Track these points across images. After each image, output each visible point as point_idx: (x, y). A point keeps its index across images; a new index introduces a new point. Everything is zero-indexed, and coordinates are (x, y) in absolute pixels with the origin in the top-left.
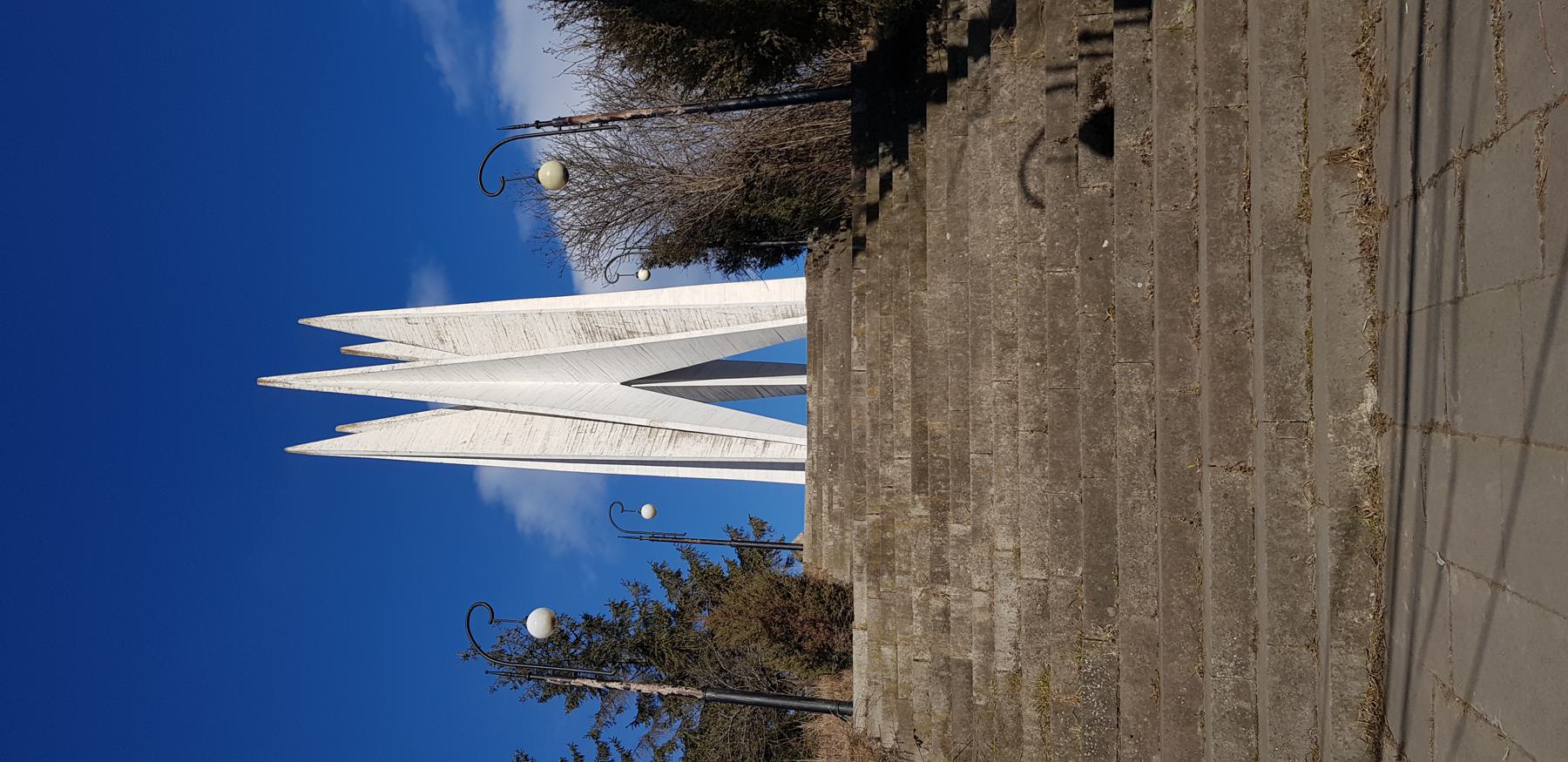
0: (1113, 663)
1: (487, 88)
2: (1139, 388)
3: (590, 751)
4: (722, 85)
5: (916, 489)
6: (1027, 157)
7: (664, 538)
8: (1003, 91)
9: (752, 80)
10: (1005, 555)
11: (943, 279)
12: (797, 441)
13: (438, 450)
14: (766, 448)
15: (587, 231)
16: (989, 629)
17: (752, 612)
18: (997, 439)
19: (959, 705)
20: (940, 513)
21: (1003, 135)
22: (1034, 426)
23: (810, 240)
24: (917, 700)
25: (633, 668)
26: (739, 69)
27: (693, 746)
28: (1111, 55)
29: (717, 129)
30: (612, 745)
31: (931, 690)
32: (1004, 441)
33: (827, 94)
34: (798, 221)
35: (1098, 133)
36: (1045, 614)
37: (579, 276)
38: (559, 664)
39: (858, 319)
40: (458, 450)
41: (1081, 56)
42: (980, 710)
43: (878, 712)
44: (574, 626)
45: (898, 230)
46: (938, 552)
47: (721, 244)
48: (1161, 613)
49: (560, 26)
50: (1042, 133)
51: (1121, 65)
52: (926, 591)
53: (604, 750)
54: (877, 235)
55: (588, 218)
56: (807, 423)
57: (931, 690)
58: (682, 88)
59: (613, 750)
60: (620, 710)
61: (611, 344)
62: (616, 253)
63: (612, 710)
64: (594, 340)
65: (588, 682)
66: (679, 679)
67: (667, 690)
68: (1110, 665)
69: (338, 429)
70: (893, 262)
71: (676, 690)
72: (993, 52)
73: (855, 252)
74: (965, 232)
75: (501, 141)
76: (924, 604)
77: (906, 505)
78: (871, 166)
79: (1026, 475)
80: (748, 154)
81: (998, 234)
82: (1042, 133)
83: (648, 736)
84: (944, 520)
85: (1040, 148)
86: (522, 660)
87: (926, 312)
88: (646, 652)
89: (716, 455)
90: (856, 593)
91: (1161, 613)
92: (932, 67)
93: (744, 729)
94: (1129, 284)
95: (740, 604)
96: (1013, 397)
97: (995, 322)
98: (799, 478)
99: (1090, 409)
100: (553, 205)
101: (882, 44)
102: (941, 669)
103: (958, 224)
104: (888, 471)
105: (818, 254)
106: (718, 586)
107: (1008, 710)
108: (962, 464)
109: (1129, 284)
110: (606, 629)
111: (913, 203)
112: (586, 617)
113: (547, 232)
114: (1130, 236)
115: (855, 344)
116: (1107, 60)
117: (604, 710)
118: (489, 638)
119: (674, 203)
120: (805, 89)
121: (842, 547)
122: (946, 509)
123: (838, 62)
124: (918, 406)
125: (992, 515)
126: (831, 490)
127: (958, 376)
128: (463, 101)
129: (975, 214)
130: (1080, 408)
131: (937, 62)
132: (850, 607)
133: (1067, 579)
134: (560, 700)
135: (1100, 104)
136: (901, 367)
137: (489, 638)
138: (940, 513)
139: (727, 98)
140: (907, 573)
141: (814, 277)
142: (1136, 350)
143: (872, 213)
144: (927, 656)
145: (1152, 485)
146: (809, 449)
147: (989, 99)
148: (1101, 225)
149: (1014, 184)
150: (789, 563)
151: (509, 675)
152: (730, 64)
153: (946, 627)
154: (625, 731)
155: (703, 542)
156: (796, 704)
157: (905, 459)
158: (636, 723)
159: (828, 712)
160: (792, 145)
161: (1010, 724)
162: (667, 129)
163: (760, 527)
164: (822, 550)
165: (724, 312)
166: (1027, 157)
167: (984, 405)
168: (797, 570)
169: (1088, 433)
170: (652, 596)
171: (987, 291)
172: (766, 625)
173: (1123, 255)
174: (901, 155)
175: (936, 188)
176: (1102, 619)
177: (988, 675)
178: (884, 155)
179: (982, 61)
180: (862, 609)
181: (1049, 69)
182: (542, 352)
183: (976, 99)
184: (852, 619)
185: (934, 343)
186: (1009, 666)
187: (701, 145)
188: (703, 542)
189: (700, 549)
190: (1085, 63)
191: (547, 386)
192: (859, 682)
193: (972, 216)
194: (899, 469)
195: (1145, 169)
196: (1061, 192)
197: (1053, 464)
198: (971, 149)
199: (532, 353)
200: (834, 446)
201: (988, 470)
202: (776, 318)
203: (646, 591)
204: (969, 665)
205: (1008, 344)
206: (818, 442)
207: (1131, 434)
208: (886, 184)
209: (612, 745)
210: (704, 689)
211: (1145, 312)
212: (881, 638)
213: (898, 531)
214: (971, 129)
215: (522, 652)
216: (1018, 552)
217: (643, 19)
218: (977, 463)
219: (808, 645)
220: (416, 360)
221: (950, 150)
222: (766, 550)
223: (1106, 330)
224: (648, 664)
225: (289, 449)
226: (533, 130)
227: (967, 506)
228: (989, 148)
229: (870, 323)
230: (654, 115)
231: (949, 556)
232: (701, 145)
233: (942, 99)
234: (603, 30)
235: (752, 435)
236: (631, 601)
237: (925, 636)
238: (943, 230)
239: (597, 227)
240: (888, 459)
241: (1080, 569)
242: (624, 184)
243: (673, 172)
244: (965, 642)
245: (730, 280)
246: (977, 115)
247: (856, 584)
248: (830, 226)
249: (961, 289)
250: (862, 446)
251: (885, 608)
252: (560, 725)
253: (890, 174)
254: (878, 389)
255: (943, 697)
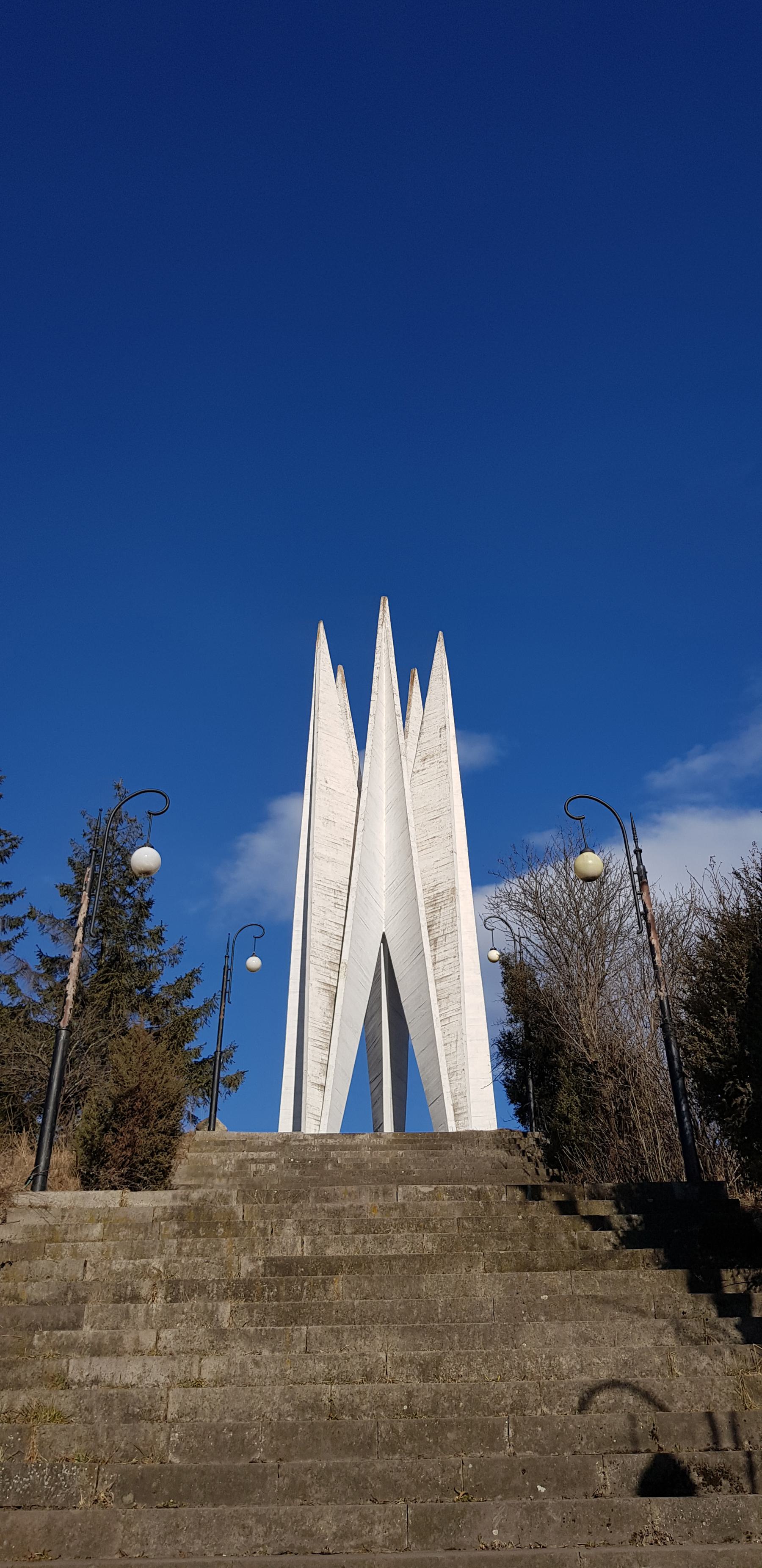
0: (71, 1501)
1: (668, 801)
2: (379, 1533)
3: (16, 910)
4: (691, 1042)
5: (269, 1261)
6: (635, 1389)
7: (226, 981)
8: (705, 1360)
9: (699, 1074)
10: (195, 1368)
11: (498, 1292)
12: (325, 1121)
13: (319, 758)
14: (316, 1095)
15: (536, 898)
16: (115, 1349)
17: (145, 1076)
18: (322, 1359)
19: (35, 1314)
20: (243, 1290)
21: (657, 1360)
22: (337, 1402)
23: (537, 1134)
24: (43, 1264)
25: (96, 951)
26: (709, 1060)
27: (13, 1015)
28: (753, 1492)
29: (647, 1032)
30: (21, 931)
31: (53, 1281)
32: (321, 1366)
33: (689, 1152)
34: (555, 1121)
35: (665, 1478)
36: (129, 1417)
37: (491, 891)
38: (105, 876)
39: (452, 1193)
40: (319, 776)
41: (749, 1455)
42: (27, 1339)
43: (33, 1219)
44: (142, 890)
45: (550, 1237)
46: (198, 1288)
47: (528, 1036)
48: (125, 1561)
49: (737, 874)
50: (662, 1408)
51: (742, 1504)
52: (159, 1275)
53: (16, 923)
54: (543, 1213)
55: (549, 900)
56: (343, 1134)
57: (53, 1281)
58: (685, 997)
59: (15, 932)
60: (55, 938)
61: (424, 923)
62: (515, 927)
63: (55, 931)
64: (427, 905)
65: (84, 908)
66: (81, 999)
67: (71, 989)
68: (69, 1498)
69: (340, 668)
70: (515, 1232)
71: (70, 998)
72: (748, 1347)
73: (524, 1188)
74: (550, 1318)
75: (618, 814)
76: (145, 1273)
77: (252, 1251)
78: (617, 1206)
79: (283, 1394)
80: (623, 1066)
81: (549, 1357)
82: (662, 1408)
83: (26, 968)
84: (235, 1295)
85: (645, 1406)
86: (111, 840)
87: (461, 1271)
88: (111, 964)
89: (310, 1033)
90: (161, 1194)
91: (125, 1561)
92: (727, 1275)
93: (26, 1069)
94: (497, 1519)
95: (155, 1063)
96: (368, 1377)
97: (451, 1356)
98: (285, 1125)
99: (354, 1472)
100: (560, 865)
101: (746, 1216)
102: (75, 1292)
103: (560, 1309)
104: (289, 1230)
105: (523, 1144)
106: (175, 1037)
107: (25, 1372)
108: (293, 1317)
109: (497, 1519)
110: (137, 923)
111: (578, 1255)
112: (150, 903)
113: (534, 860)
114: (550, 1520)
115: (426, 1189)
116: (747, 1487)
117: (56, 922)
118: (135, 809)
119: (568, 987)
120: (694, 1128)
121: (211, 1175)
122: (247, 1297)
123: (725, 1167)
124: (359, 1264)
125: (239, 1352)
126: (271, 1161)
127: (392, 1310)
128: (658, 780)
129: (569, 1329)
130: (357, 1459)
131: (733, 1281)
132: (146, 1186)
133: (167, 1444)
134: (70, 879)
135: (697, 1479)
136: (402, 1243)
137: (135, 809)
138: (243, 1290)
139: (679, 1046)
140: (179, 1253)
141: (499, 1139)
142: (422, 1529)
143: (567, 1207)
144: (89, 1277)
145: (270, 1550)
146: (315, 1136)
147: (696, 1343)
148: (564, 1482)
149: (604, 1375)
150: (194, 1119)
151: (96, 829)
152: (713, 1049)
153: (119, 1299)
154: (33, 945)
155: (221, 1022)
156: (48, 1127)
157: (302, 1249)
158: (41, 955)
159: (37, 1162)
160: (635, 1114)
161: (11, 1376)
162: (643, 980)
163: (232, 1083)
164: (209, 1151)
165: (458, 1040)
166: (635, 1389)
167: (360, 1342)
168: (187, 1127)
169: (329, 1470)
170: (167, 969)
171: (485, 1345)
172: (132, 1092)
173: (529, 1510)
174: (630, 1240)
175: (595, 1282)
176: (120, 1487)
177: (66, 1349)
178: (630, 1220)
179: (736, 1334)
180: (144, 1201)
181: (733, 1415)
182: (415, 854)
183: (696, 1327)
184: (133, 1189)
185: (428, 1282)
186: (73, 1374)
187: (629, 1014)
188: (221, 1022)
189: (214, 1019)
190: (742, 1459)
191: (382, 861)
192: (67, 1198)
193: (568, 1325)
194: (292, 1242)
195: (627, 1536)
196: (597, 1433)
197: (294, 1427)
198: (640, 1322)
199: (414, 845)
200: (318, 1164)
201: (289, 1347)
202: (454, 1096)
203: (174, 962)
204: (76, 1326)
205: (428, 1370)
206: (322, 1146)
207: (327, 1522)
208: (599, 1223)
209: (21, 931)
210: (70, 1029)
211: (465, 1540)
212: (112, 1223)
213: (225, 1242)
214: (662, 1323)
215: (119, 840)
216: (198, 1384)
217: (751, 958)
218: (296, 1335)
219: (108, 1138)
220: (406, 736)
221: (638, 1298)
222: (210, 1091)
223: (444, 1491)
224: (100, 967)
225: (321, 625)
226: (632, 848)
227: (249, 1322)
228: (643, 1345)
229: (447, 1206)
230: (655, 967)
231: (197, 1301)
232: (629, 1014)
233: (694, 1287)
234: (737, 917)
235: (331, 1071)
236: (165, 947)
237: (111, 1273)
238: (551, 1291)
239: (539, 908)
240: (302, 1228)
241: (176, 1461)
242: (584, 935)
243: (600, 986)
244: (102, 1321)
245: (491, 1046)
246: (677, 1330)
247: (170, 1193)
248: (553, 1157)
249: (486, 1314)
250: (317, 1199)
251: (143, 1227)
252: (41, 878)
253: (610, 1228)
254: (378, 1216)
255: (44, 1296)
